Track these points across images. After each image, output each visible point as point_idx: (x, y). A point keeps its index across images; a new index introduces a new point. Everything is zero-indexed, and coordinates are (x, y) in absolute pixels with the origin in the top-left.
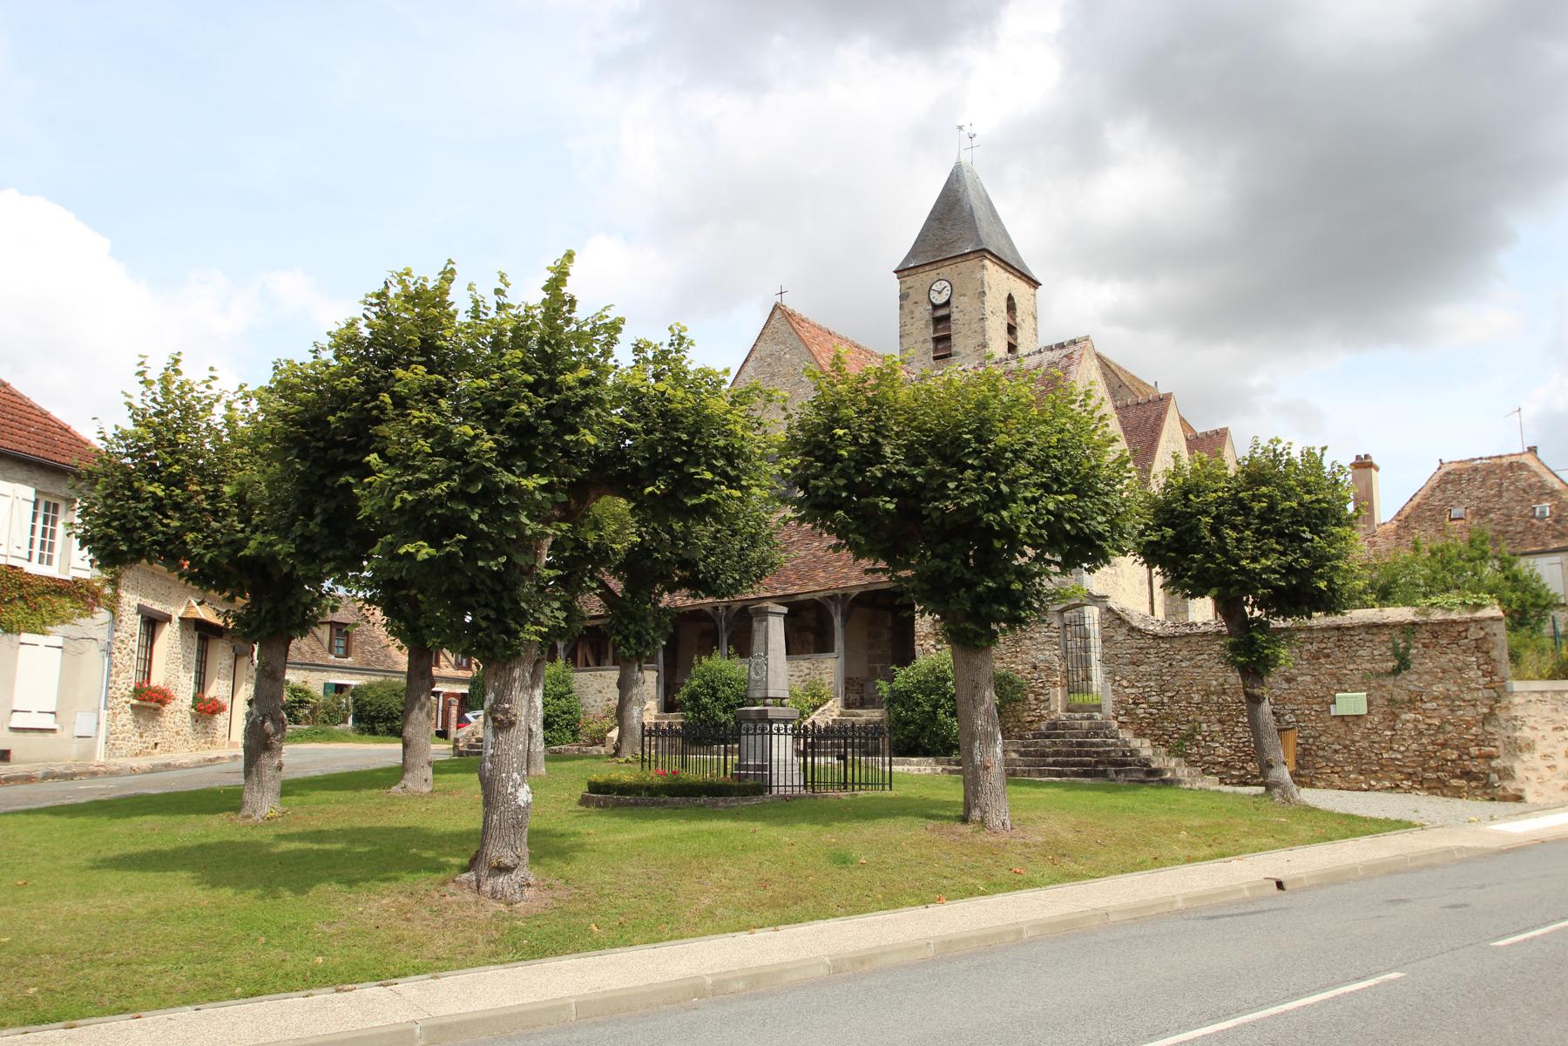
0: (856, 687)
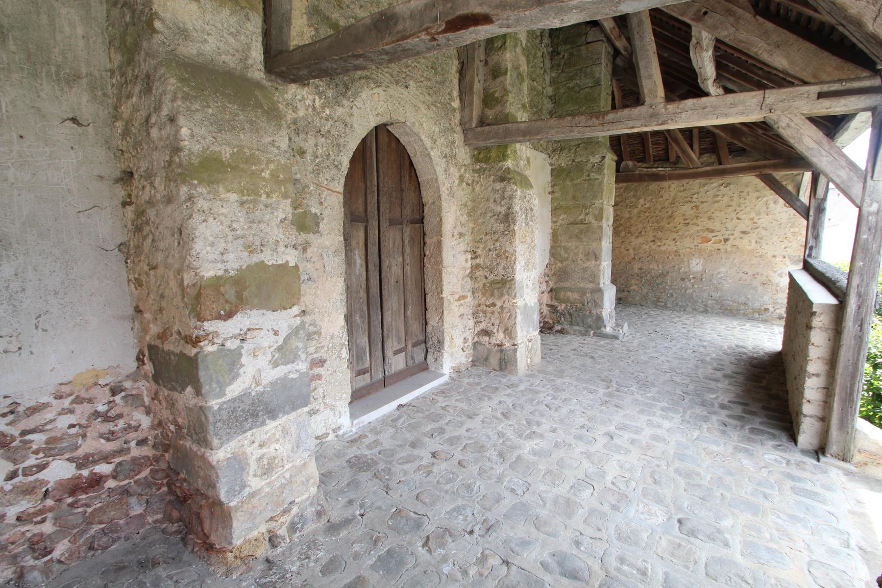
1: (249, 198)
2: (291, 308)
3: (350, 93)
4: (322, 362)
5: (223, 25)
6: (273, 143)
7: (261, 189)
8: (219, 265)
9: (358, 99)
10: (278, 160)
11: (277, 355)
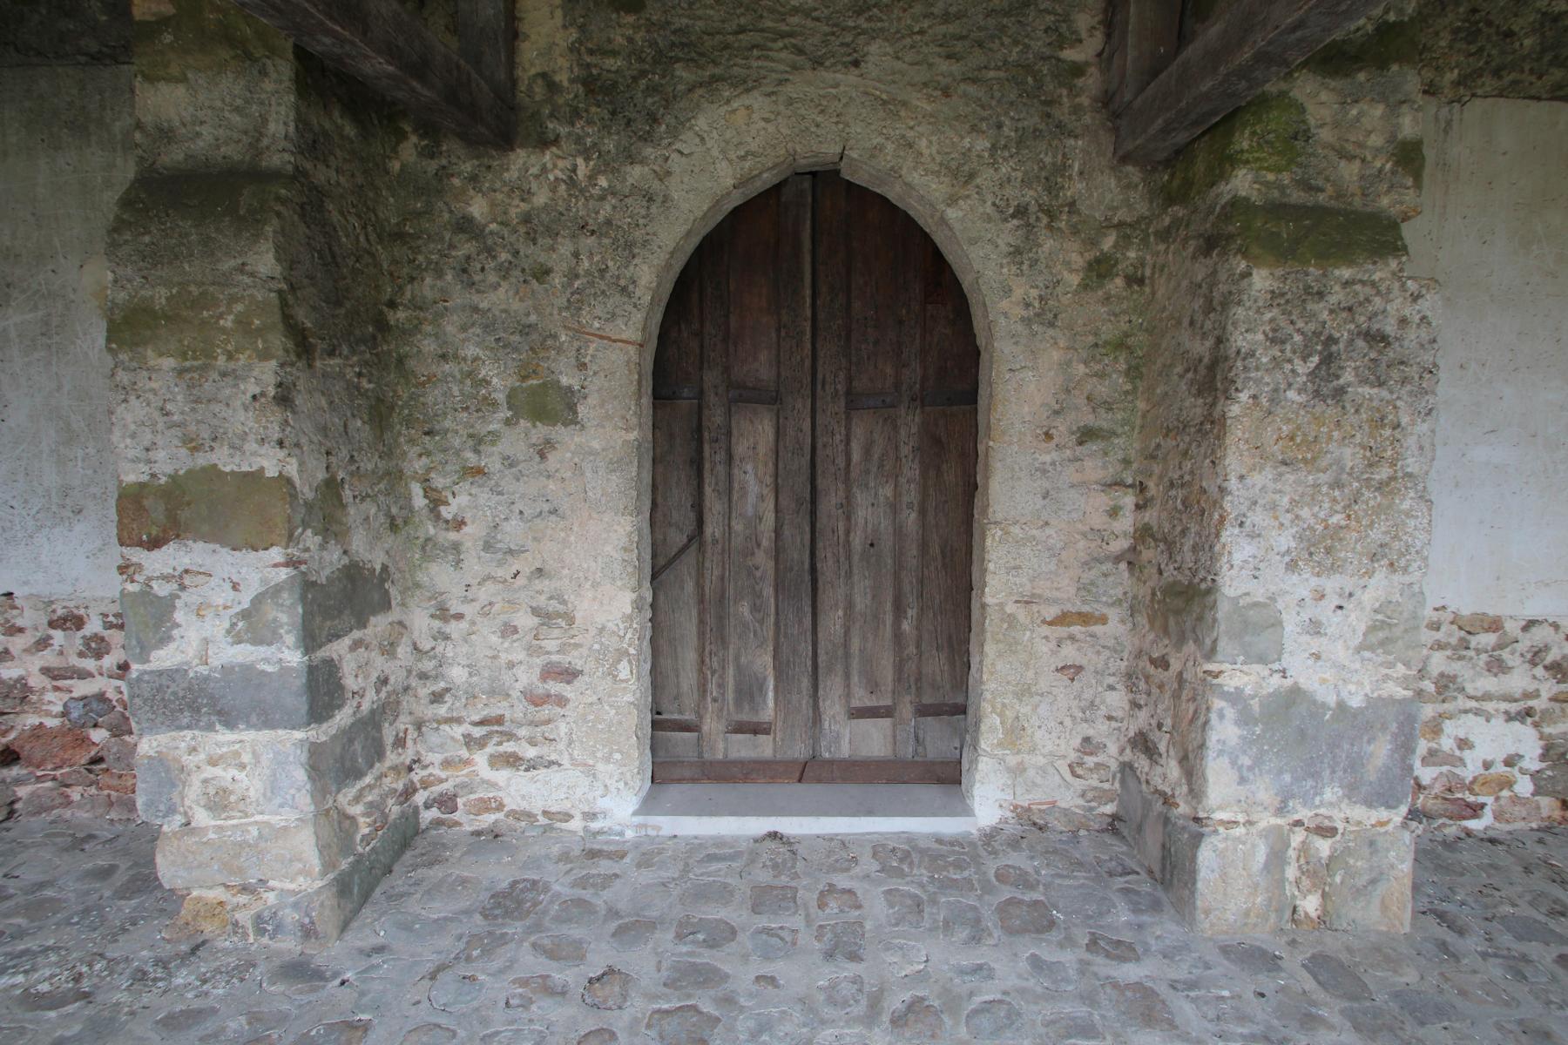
0: (1519, 680)
1: (196, 363)
2: (266, 549)
3: (664, 127)
4: (569, 674)
5: (223, 101)
6: (241, 269)
7: (218, 346)
8: (145, 468)
9: (687, 135)
10: (251, 296)
11: (240, 624)
